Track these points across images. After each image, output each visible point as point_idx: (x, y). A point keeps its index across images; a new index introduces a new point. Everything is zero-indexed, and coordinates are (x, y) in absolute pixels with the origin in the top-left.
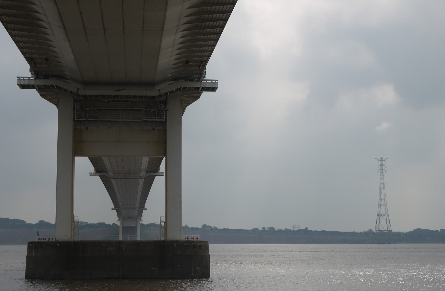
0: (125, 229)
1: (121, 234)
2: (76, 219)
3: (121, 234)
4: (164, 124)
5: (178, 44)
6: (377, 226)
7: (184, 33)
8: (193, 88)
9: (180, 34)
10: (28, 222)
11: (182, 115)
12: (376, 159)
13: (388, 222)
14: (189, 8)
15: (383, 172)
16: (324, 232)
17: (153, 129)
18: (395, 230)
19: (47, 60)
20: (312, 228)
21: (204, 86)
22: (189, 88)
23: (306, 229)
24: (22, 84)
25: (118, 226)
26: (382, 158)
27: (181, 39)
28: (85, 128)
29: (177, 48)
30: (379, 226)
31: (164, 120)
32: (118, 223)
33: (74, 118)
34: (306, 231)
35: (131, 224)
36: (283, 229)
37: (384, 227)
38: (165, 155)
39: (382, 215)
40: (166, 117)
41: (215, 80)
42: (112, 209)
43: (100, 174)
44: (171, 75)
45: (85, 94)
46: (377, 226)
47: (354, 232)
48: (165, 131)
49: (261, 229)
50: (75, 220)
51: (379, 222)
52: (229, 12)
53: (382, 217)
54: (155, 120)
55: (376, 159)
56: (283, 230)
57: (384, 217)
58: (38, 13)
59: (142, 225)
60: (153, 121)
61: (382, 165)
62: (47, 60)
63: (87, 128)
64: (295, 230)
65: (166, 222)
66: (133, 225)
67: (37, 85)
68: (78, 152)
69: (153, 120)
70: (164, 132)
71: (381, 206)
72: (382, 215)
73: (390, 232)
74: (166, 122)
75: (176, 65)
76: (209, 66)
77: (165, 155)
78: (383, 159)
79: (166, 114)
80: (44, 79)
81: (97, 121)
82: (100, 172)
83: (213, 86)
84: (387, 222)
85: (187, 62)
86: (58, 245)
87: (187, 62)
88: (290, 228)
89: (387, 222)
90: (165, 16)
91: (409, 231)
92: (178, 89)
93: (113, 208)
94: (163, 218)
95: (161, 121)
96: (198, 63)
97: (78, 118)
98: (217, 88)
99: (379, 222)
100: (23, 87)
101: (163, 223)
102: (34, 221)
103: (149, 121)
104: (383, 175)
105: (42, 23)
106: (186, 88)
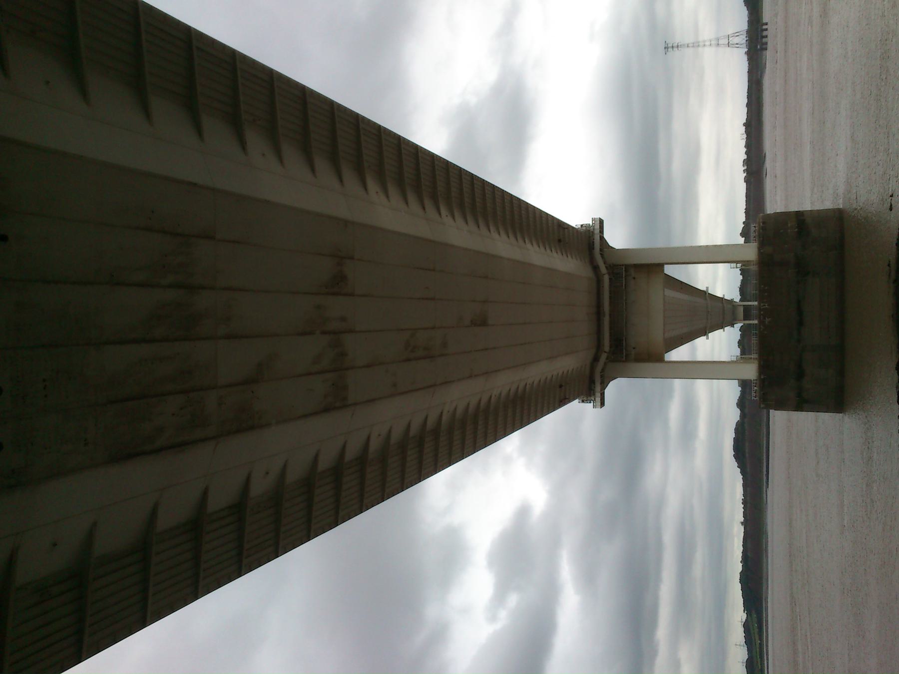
1: (751, 322)
2: (734, 359)
3: (751, 322)
4: (627, 267)
6: (741, 46)
8: (600, 242)
9: (529, 246)
15: (681, 45)
16: (748, 105)
19: (561, 386)
20: (743, 118)
22: (601, 246)
24: (600, 404)
31: (624, 268)
33: (623, 361)
34: (747, 125)
37: (742, 39)
38: (660, 266)
39: (729, 42)
41: (593, 221)
46: (741, 46)
47: (741, 274)
49: (745, 174)
50: (735, 360)
51: (737, 44)
52: (460, 170)
53: (730, 42)
56: (746, 150)
57: (730, 39)
58: (518, 388)
59: (741, 300)
61: (673, 47)
62: (561, 386)
63: (634, 348)
64: (746, 136)
65: (737, 262)
66: (742, 309)
67: (601, 390)
68: (660, 359)
69: (624, 279)
71: (718, 44)
72: (729, 42)
73: (748, 32)
78: (666, 46)
79: (618, 265)
80: (595, 384)
81: (625, 338)
83: (599, 222)
84: (737, 36)
85: (560, 241)
86: (762, 377)
87: (560, 241)
88: (743, 143)
89: (737, 36)
90: (508, 259)
93: (705, 337)
94: (732, 265)
95: (625, 271)
98: (600, 218)
99: (737, 44)
101: (738, 265)
103: (625, 282)
104: (684, 45)
106: (600, 249)
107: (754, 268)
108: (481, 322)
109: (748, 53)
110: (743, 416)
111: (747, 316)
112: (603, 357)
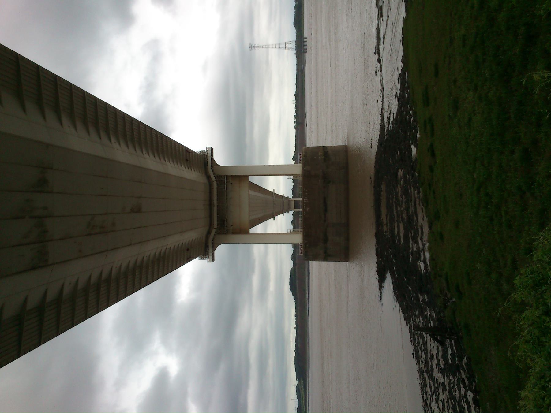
0: (296, 207)
4: (227, 177)
5: (121, 147)
7: (144, 152)
8: (211, 162)
9: (168, 163)
10: (292, 267)
11: (219, 165)
12: (250, 50)
13: (290, 43)
14: (149, 155)
15: (259, 46)
17: (231, 184)
18: (294, 39)
19: (188, 250)
21: (210, 155)
22: (211, 164)
23: (295, 95)
24: (212, 260)
25: (294, 212)
26: (250, 47)
27: (156, 157)
28: (232, 227)
29: (177, 165)
30: (293, 49)
31: (225, 177)
32: (292, 212)
33: (225, 234)
34: (296, 117)
35: (293, 203)
36: (295, 110)
37: (293, 45)
38: (247, 177)
39: (286, 47)
40: (223, 176)
41: (207, 148)
42: (283, 215)
43: (274, 216)
44: (167, 161)
45: (217, 224)
48: (233, 177)
51: (290, 48)
54: (225, 182)
55: (250, 50)
57: (287, 45)
59: (293, 197)
60: (226, 184)
63: (232, 226)
64: (295, 102)
65: (290, 175)
66: (293, 203)
69: (225, 184)
70: (234, 177)
72: (286, 47)
74: (226, 176)
75: (161, 158)
76: (271, 191)
77: (247, 177)
78: (251, 46)
79: (222, 176)
80: (208, 248)
82: (273, 216)
83: (210, 149)
85: (187, 160)
86: (305, 242)
87: (187, 160)
88: (294, 106)
91: (295, 28)
92: (212, 171)
93: (273, 219)
95: (226, 179)
96: (188, 153)
97: (225, 231)
98: (211, 147)
99: (290, 48)
100: (213, 260)
101: (291, 176)
102: (292, 263)
104: (261, 46)
105: (162, 251)
106: (211, 166)
107: (300, 179)
108: (137, 210)
109: (296, 54)
110: (294, 265)
111: (296, 207)
112: (214, 231)
